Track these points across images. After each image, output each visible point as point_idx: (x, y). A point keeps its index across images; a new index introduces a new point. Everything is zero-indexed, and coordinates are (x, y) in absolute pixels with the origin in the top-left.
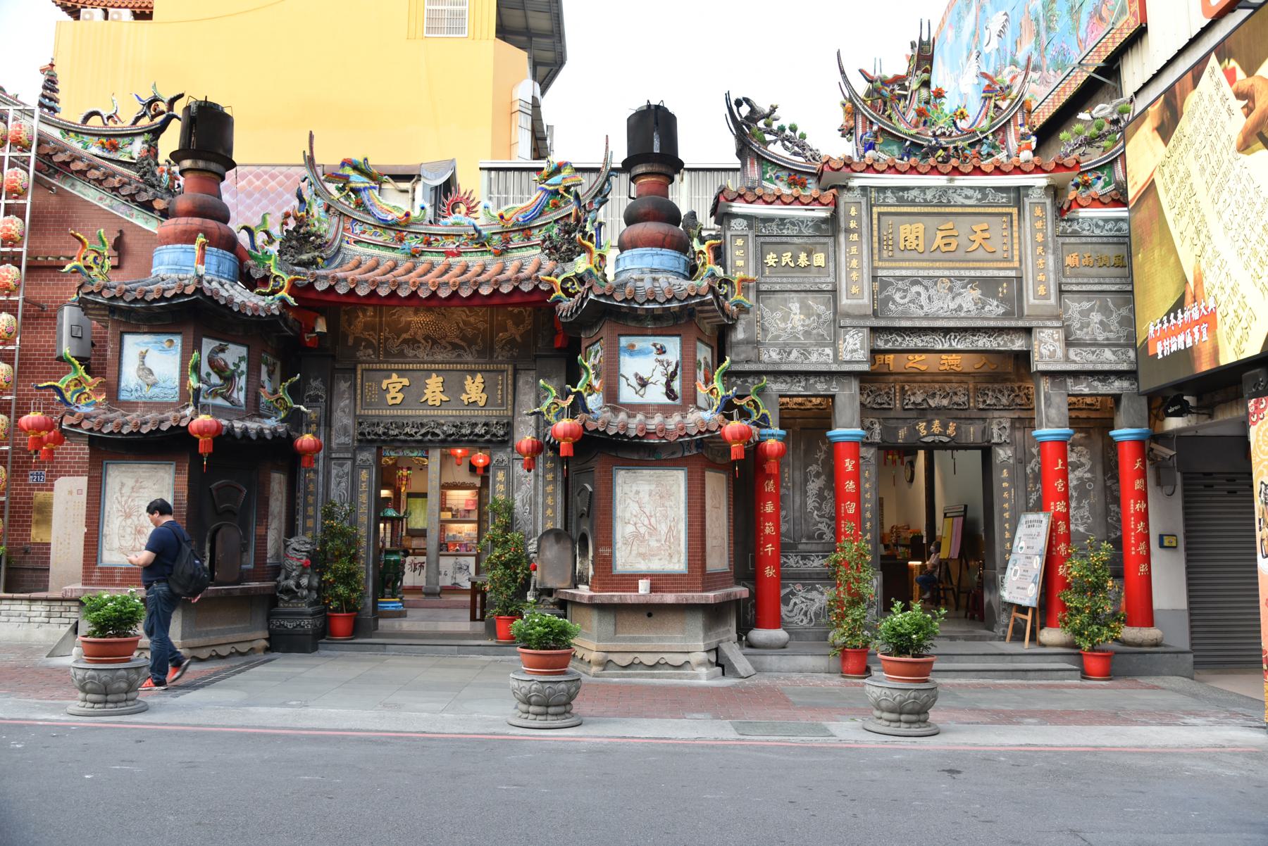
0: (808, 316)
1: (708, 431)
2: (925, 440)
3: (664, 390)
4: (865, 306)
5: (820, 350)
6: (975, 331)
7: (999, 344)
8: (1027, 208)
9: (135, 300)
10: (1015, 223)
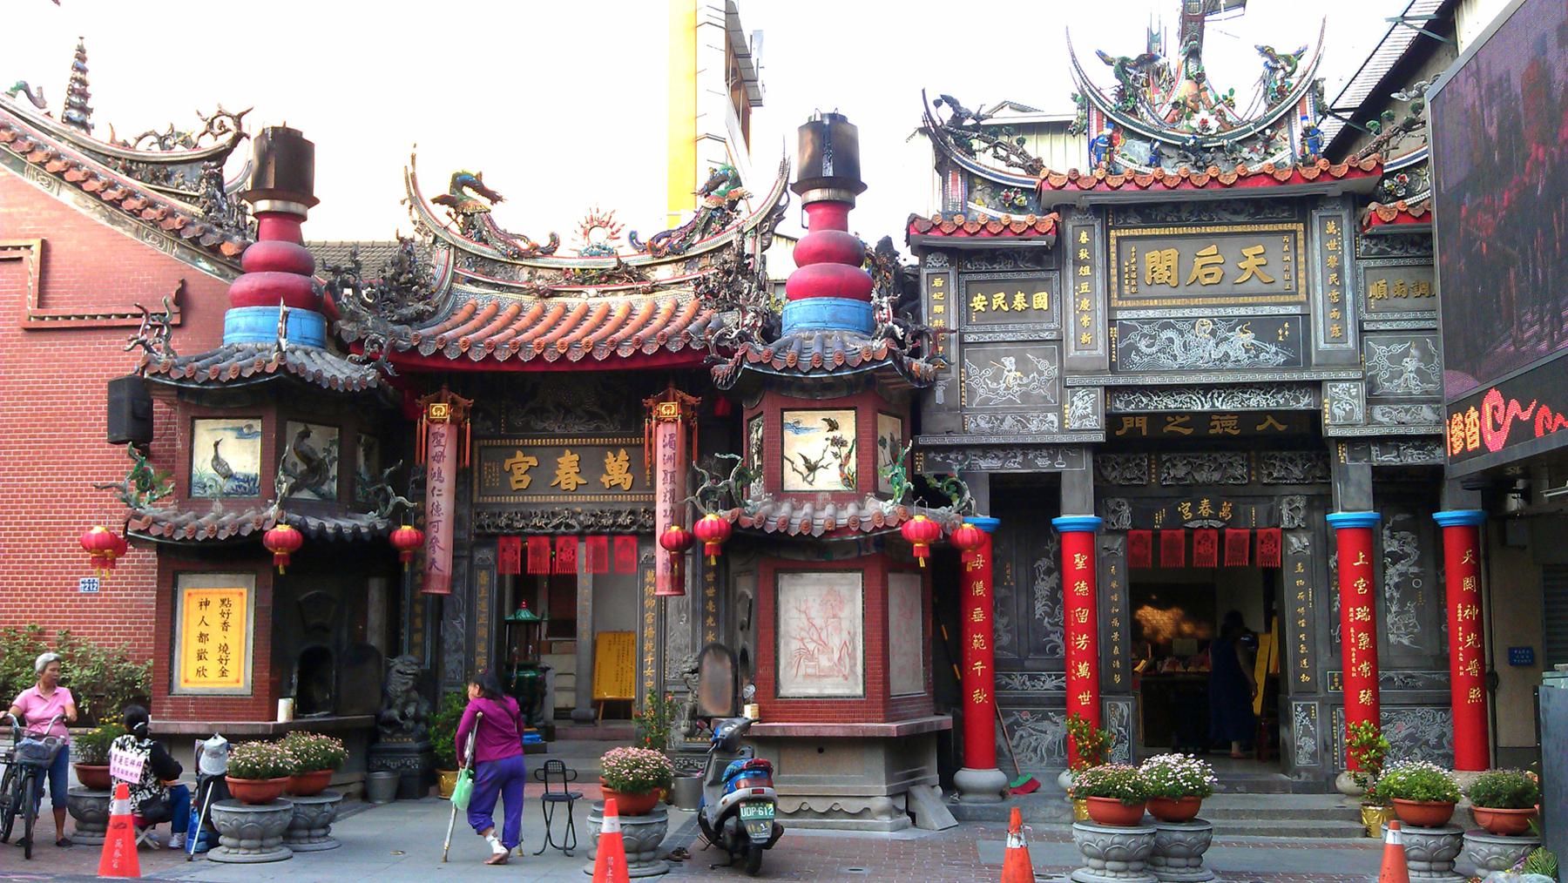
1: (886, 527)
2: (1190, 525)
4: (1099, 358)
6: (1245, 387)
7: (1277, 402)
9: (208, 382)
10: (1301, 243)
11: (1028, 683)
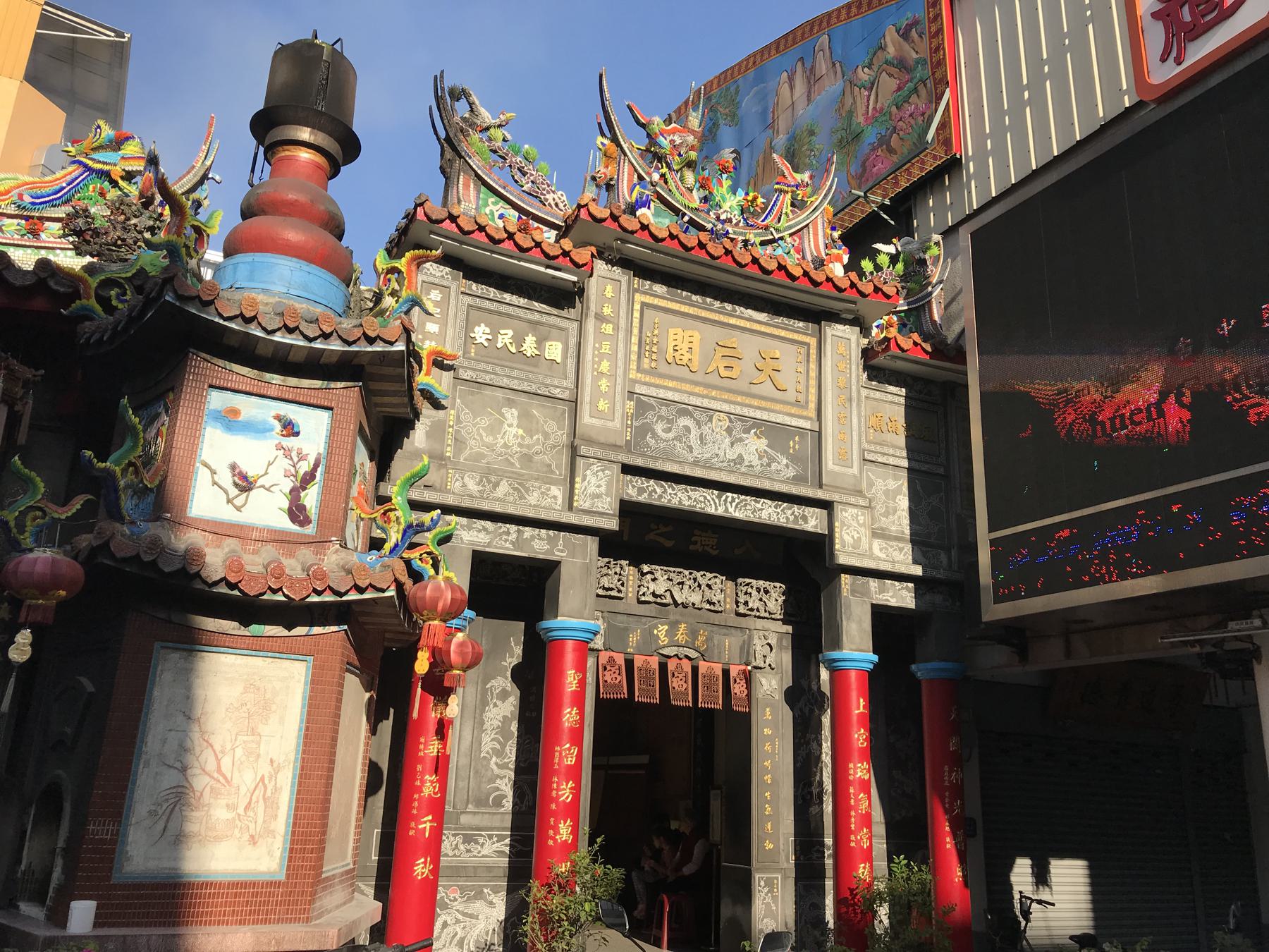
0: (530, 433)
2: (666, 651)
3: (286, 505)
5: (545, 487)
7: (787, 518)
8: (829, 340)
11: (462, 847)
